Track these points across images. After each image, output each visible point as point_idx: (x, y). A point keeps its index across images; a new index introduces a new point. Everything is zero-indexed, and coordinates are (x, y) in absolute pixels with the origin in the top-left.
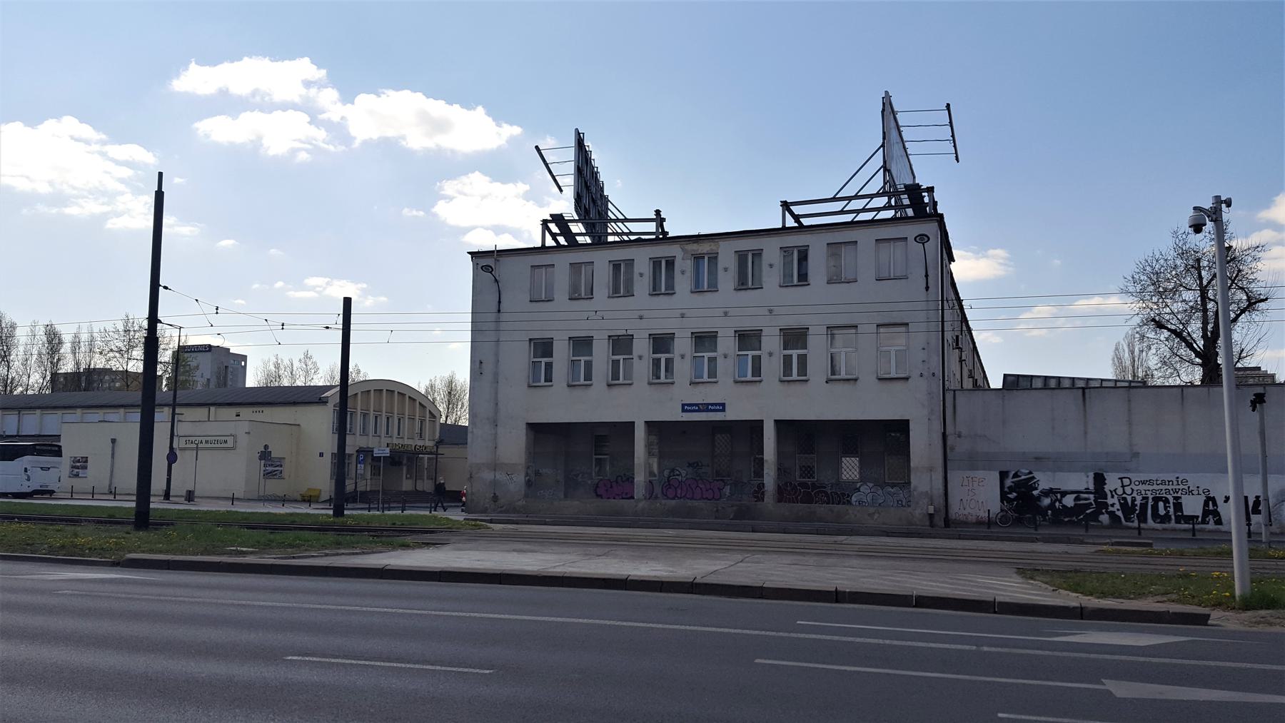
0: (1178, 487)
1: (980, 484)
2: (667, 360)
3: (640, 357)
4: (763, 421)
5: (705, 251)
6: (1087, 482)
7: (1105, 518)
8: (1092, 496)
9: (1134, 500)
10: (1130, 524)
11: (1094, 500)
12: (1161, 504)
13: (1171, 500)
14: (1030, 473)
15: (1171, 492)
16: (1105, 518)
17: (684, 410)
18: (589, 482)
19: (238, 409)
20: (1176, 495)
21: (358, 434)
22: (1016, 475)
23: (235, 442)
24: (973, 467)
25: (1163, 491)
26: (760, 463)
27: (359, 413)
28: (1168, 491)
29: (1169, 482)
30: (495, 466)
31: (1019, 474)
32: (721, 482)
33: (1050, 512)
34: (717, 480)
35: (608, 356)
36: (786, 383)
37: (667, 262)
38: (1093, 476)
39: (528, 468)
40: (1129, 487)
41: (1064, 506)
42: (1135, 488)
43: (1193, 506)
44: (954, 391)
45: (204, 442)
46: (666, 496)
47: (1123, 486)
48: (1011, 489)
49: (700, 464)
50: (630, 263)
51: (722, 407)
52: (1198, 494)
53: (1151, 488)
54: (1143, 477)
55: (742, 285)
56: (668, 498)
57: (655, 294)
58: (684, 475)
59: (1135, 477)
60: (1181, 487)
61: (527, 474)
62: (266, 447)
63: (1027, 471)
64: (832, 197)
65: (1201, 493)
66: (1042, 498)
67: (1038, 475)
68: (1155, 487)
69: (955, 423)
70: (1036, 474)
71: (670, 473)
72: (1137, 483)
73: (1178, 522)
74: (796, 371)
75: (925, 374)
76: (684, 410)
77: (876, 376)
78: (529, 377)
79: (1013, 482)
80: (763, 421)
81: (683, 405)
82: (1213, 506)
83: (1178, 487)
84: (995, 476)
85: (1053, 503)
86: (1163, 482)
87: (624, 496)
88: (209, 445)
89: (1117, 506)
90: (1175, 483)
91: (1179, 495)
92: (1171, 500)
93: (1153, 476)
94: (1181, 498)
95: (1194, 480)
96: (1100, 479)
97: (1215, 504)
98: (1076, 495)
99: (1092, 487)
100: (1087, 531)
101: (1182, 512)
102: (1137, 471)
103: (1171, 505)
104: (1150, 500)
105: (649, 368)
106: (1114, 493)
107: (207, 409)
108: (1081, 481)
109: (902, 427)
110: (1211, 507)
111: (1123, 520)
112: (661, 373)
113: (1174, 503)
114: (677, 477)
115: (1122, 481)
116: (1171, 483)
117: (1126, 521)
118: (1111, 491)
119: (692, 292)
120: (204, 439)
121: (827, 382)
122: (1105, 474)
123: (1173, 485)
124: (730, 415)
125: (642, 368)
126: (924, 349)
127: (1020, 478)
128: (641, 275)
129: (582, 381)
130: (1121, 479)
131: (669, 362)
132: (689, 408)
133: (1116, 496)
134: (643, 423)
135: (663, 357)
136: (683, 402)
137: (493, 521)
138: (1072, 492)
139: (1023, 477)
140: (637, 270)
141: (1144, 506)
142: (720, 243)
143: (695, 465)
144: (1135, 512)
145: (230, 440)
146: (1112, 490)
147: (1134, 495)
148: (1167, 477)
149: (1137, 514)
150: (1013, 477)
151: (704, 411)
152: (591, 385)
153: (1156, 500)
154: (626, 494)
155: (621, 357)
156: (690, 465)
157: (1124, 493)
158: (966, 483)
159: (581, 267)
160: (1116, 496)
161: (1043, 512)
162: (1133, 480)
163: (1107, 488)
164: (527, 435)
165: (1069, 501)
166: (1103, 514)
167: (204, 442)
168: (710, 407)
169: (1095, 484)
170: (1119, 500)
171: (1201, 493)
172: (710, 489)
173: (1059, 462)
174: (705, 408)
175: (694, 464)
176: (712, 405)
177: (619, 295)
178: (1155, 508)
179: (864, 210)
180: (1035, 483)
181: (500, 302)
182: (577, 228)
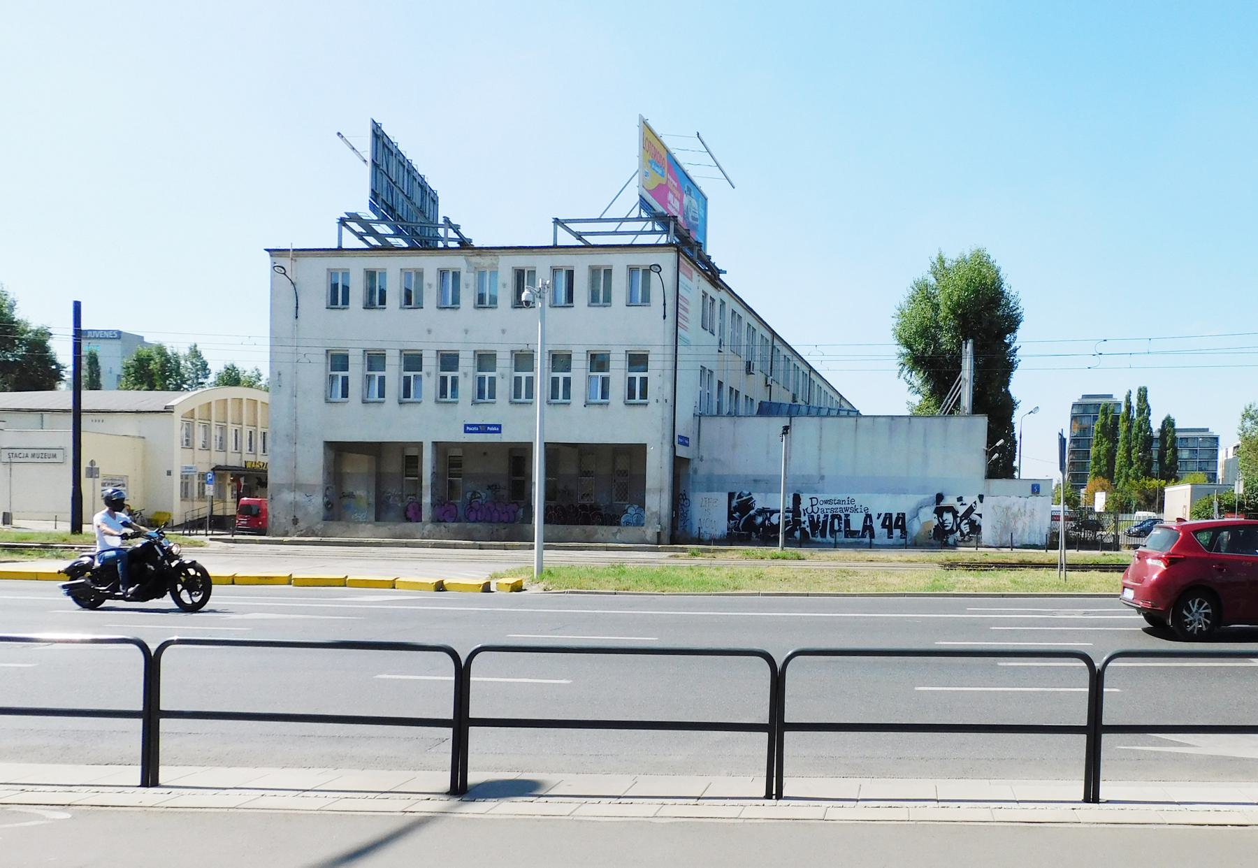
2: (380, 378)
3: (428, 374)
7: (797, 534)
8: (791, 514)
9: (818, 518)
11: (792, 519)
12: (836, 521)
13: (843, 518)
14: (750, 494)
16: (797, 534)
17: (466, 431)
20: (846, 513)
21: (213, 449)
22: (740, 497)
24: (710, 490)
25: (839, 510)
31: (742, 495)
32: (515, 505)
34: (513, 503)
35: (400, 374)
38: (792, 496)
39: (327, 489)
41: (771, 524)
42: (820, 507)
43: (857, 523)
45: (30, 455)
46: (468, 518)
47: (812, 506)
48: (736, 509)
51: (498, 428)
53: (830, 506)
56: (470, 522)
58: (484, 498)
59: (822, 497)
60: (850, 506)
61: (326, 496)
63: (748, 493)
67: (755, 496)
68: (834, 506)
71: (472, 495)
72: (821, 503)
73: (846, 536)
74: (559, 392)
75: (660, 400)
76: (466, 431)
77: (623, 401)
78: (326, 391)
81: (466, 426)
84: (724, 497)
85: (764, 522)
88: (35, 460)
89: (807, 523)
90: (847, 502)
91: (848, 513)
92: (843, 518)
93: (832, 497)
95: (862, 500)
96: (797, 499)
97: (871, 521)
101: (849, 528)
103: (843, 522)
104: (829, 517)
109: (642, 448)
110: (868, 524)
111: (810, 535)
112: (446, 390)
122: (801, 495)
124: (507, 436)
128: (430, 285)
130: (811, 499)
131: (455, 380)
132: (471, 429)
133: (807, 514)
134: (430, 444)
135: (449, 375)
136: (466, 423)
137: (238, 541)
139: (745, 498)
141: (825, 522)
142: (500, 257)
149: (820, 530)
150: (737, 499)
152: (383, 402)
153: (834, 517)
155: (411, 374)
156: (489, 487)
157: (813, 511)
160: (807, 514)
162: (819, 501)
163: (802, 507)
164: (325, 454)
167: (30, 455)
172: (507, 512)
173: (768, 484)
174: (483, 429)
178: (832, 524)
181: (297, 307)
182: (383, 229)
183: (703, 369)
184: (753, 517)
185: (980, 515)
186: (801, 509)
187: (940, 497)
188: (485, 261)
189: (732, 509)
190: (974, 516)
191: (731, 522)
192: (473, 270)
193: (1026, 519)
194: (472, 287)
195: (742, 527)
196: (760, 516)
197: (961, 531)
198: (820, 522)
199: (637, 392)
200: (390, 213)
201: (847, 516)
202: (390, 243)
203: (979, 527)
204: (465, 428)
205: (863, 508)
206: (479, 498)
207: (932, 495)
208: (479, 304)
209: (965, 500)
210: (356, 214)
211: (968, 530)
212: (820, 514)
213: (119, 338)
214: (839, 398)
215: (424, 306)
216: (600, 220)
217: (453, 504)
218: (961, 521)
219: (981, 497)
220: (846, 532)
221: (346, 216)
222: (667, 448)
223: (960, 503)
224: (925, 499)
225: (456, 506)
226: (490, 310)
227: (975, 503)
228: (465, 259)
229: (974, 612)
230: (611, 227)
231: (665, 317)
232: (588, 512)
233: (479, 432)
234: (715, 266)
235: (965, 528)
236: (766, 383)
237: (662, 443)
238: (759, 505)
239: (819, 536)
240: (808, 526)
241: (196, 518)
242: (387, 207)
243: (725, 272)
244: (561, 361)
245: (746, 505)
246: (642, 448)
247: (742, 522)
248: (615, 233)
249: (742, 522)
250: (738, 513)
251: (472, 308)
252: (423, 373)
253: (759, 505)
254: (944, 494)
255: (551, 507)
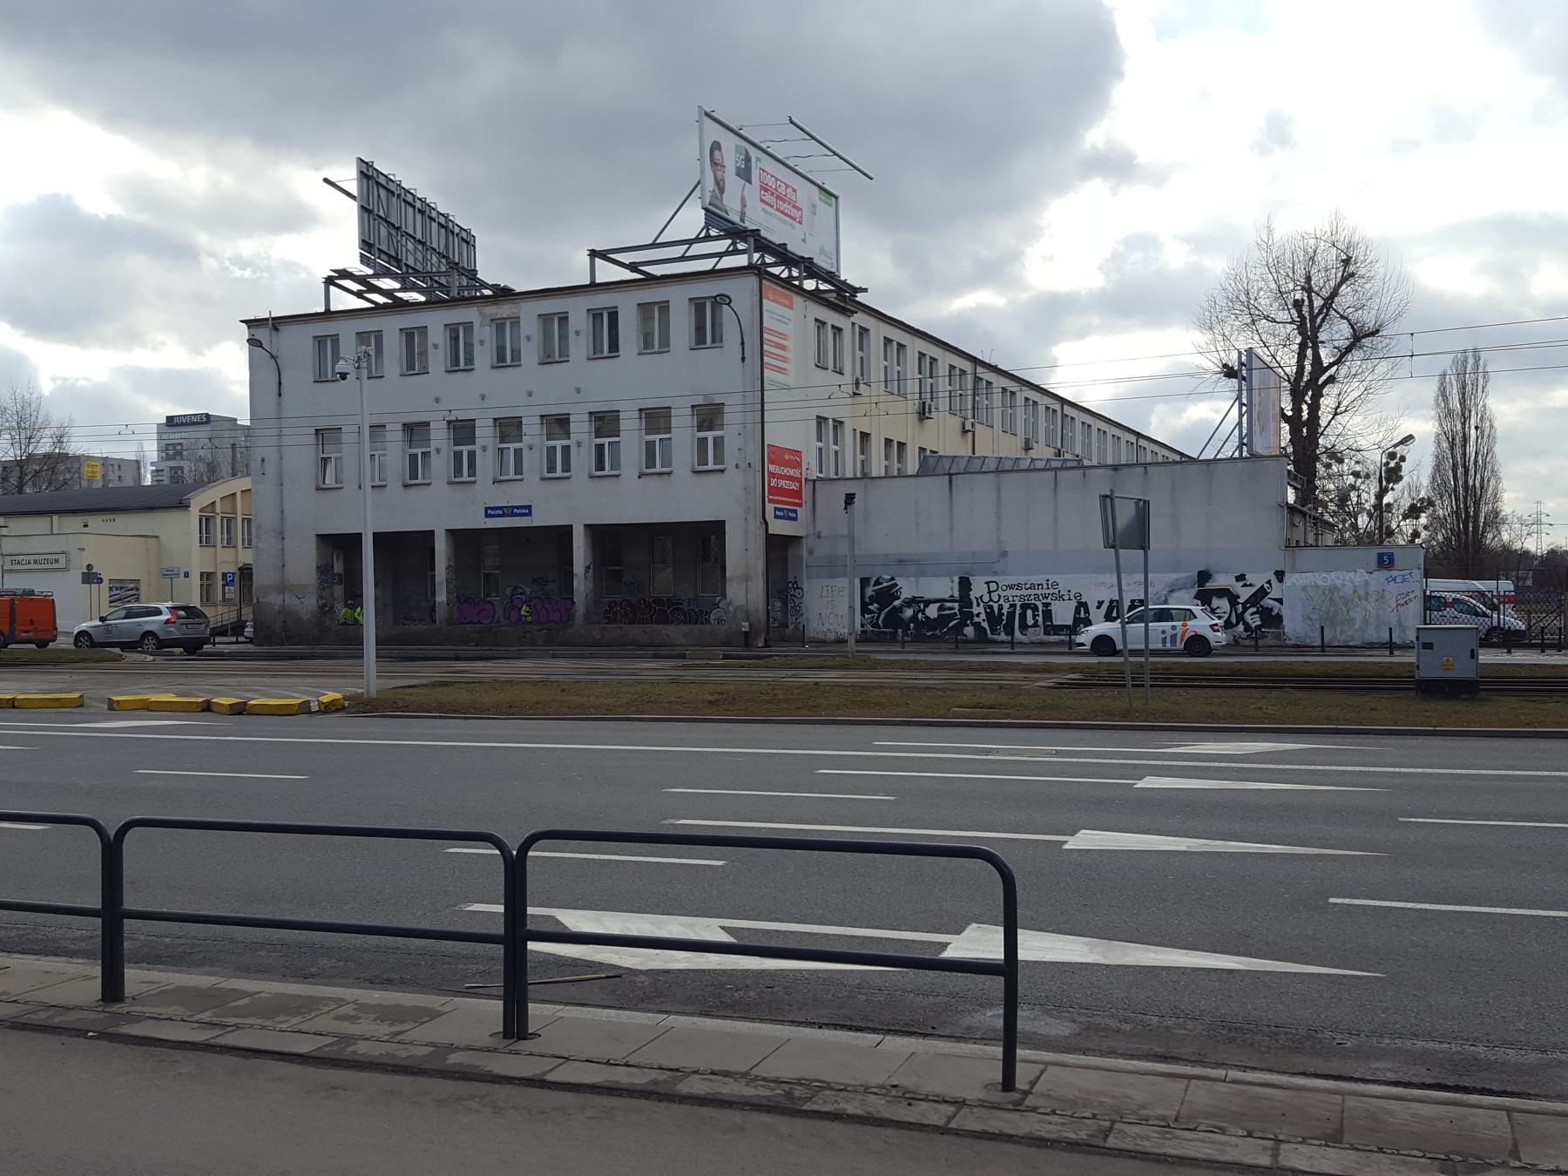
0: (1048, 591)
1: (840, 594)
2: (566, 449)
4: (572, 526)
5: (505, 316)
6: (952, 589)
7: (969, 631)
8: (956, 605)
9: (1001, 607)
10: (995, 637)
11: (959, 610)
12: (1029, 612)
13: (1040, 607)
14: (892, 579)
15: (1041, 597)
16: (969, 631)
17: (487, 516)
18: (423, 605)
19: (84, 517)
20: (1045, 601)
21: (219, 545)
22: (877, 583)
23: (68, 561)
25: (1032, 597)
26: (570, 575)
27: (240, 521)
28: (1037, 597)
29: (1038, 585)
30: (283, 588)
32: (568, 601)
33: (912, 625)
36: (596, 479)
37: (560, 319)
40: (997, 593)
41: (927, 618)
42: (1002, 594)
43: (1063, 614)
44: (814, 481)
45: (32, 561)
47: (990, 592)
48: (873, 600)
49: (545, 580)
50: (423, 330)
52: (1069, 599)
53: (1019, 593)
54: (1013, 580)
55: (454, 367)
57: (595, 359)
58: (528, 593)
59: (1003, 580)
60: (1051, 591)
62: (89, 567)
64: (651, 242)
65: (1072, 597)
66: (905, 608)
68: (1024, 592)
69: (814, 521)
70: (899, 581)
71: (513, 591)
72: (1004, 588)
75: (741, 464)
76: (487, 516)
79: (874, 591)
80: (572, 526)
81: (487, 509)
82: (1085, 614)
83: (1048, 591)
85: (915, 615)
86: (1032, 587)
87: (463, 621)
88: (38, 566)
89: (983, 616)
90: (1045, 586)
91: (1049, 601)
92: (1040, 607)
93: (1022, 580)
94: (1050, 604)
95: (1066, 582)
96: (965, 584)
97: (1087, 611)
98: (939, 604)
99: (956, 594)
100: (903, 647)
102: (1004, 573)
103: (1040, 613)
104: (1018, 608)
105: (448, 463)
106: (980, 601)
107: (49, 518)
108: (942, 588)
109: (718, 527)
110: (1082, 615)
111: (989, 632)
112: (463, 468)
113: (1043, 610)
114: (520, 596)
115: (989, 587)
116: (1040, 587)
117: (992, 634)
118: (977, 599)
119: (589, 359)
120: (32, 558)
121: (639, 477)
123: (1042, 588)
124: (538, 519)
125: (441, 465)
126: (739, 434)
127: (881, 586)
128: (436, 346)
129: (512, 476)
130: (988, 583)
131: (472, 455)
132: (518, 511)
133: (982, 604)
135: (465, 449)
138: (937, 601)
139: (885, 584)
140: (431, 340)
141: (1011, 615)
143: (541, 581)
144: (1001, 623)
145: (62, 558)
146: (978, 596)
147: (1001, 602)
148: (1036, 580)
149: (1004, 625)
150: (874, 586)
151: (508, 516)
153: (1024, 607)
154: (465, 618)
155: (605, 441)
156: (535, 581)
157: (991, 600)
158: (825, 594)
159: (370, 337)
160: (982, 604)
161: (904, 625)
163: (973, 595)
164: (318, 549)
165: (932, 611)
166: (968, 625)
167: (32, 561)
168: (515, 510)
169: (959, 591)
170: (985, 609)
171: (1072, 597)
173: (920, 566)
174: (509, 511)
175: (539, 579)
176: (517, 507)
177: (414, 372)
178: (1023, 617)
179: (720, 255)
180: (897, 591)
181: (280, 383)
183: (821, 420)
184: (900, 609)
185: (1280, 601)
186: (972, 597)
187: (1204, 576)
188: (504, 310)
189: (867, 600)
190: (1267, 602)
191: (867, 616)
192: (488, 322)
193: (1371, 606)
194: (487, 344)
195: (883, 622)
196: (909, 607)
197: (1246, 624)
198: (1003, 615)
199: (708, 459)
200: (395, 264)
201: (1046, 605)
202: (401, 299)
203: (1279, 618)
204: (486, 512)
205: (1072, 594)
206: (521, 594)
207: (1189, 574)
208: (498, 362)
209: (1250, 578)
210: (345, 270)
211: (1259, 623)
212: (1005, 599)
213: (208, 422)
214: (1135, 438)
215: (430, 371)
216: (654, 245)
217: (489, 602)
218: (1245, 609)
219: (1280, 575)
220: (1046, 627)
221: (334, 274)
222: (755, 526)
223: (1241, 583)
224: (1177, 579)
225: (494, 606)
226: (511, 368)
227: (1269, 582)
228: (478, 311)
229: (404, 669)
230: (678, 251)
231: (743, 359)
232: (665, 608)
233: (503, 515)
234: (848, 284)
235: (1254, 620)
236: (964, 428)
237: (746, 519)
238: (907, 592)
239: (1003, 634)
240: (984, 620)
241: (220, 624)
242: (389, 259)
243: (865, 290)
244: (463, 431)
245: (886, 595)
246: (718, 527)
247: (882, 617)
248: (683, 258)
249: (882, 617)
250: (876, 605)
251: (443, 372)
252: (477, 447)
253: (907, 592)
254: (1211, 572)
255: (615, 602)
